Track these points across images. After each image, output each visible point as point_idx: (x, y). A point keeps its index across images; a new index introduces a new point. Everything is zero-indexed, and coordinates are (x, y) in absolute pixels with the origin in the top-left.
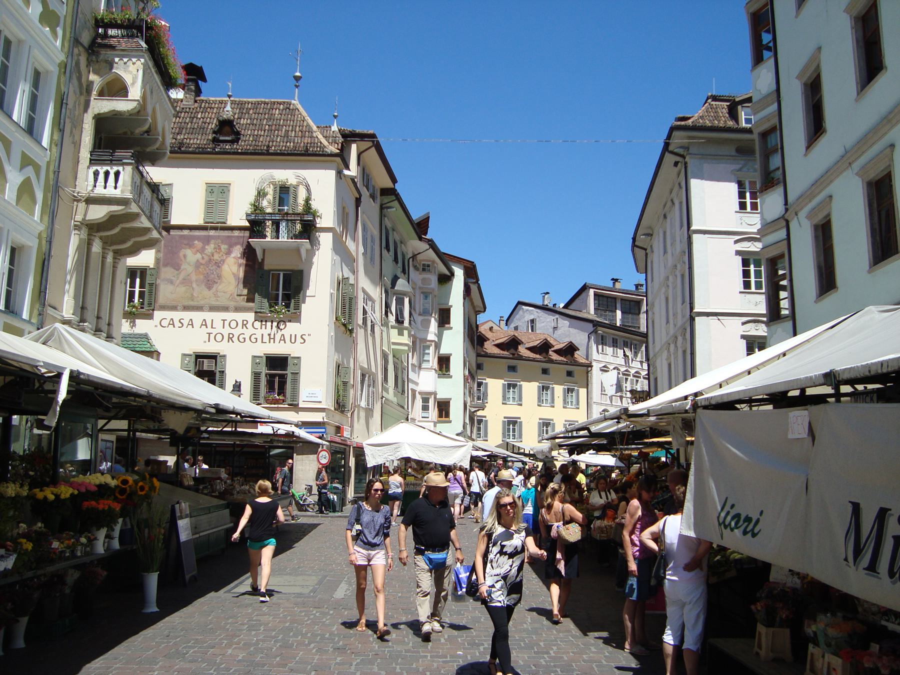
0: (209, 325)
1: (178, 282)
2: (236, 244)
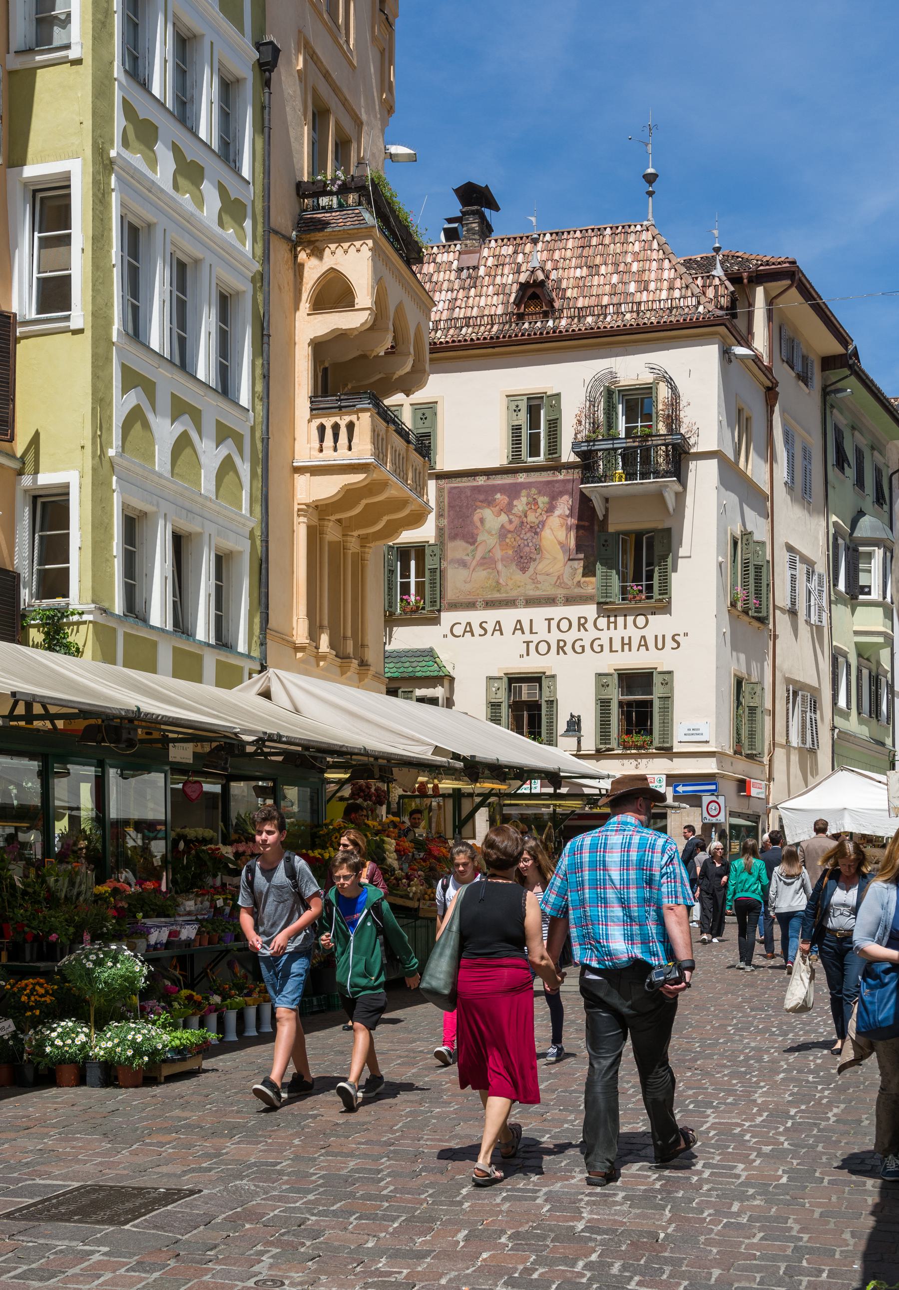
0: (526, 628)
1: (474, 563)
2: (561, 494)
